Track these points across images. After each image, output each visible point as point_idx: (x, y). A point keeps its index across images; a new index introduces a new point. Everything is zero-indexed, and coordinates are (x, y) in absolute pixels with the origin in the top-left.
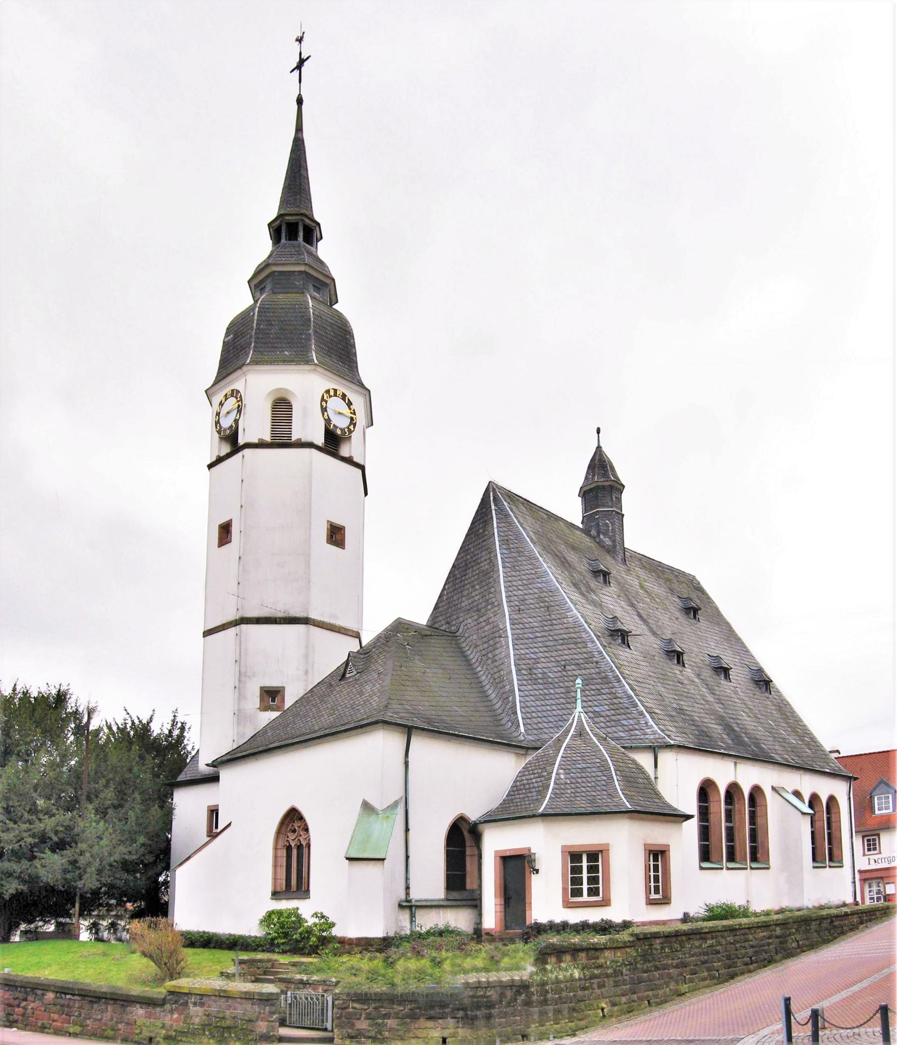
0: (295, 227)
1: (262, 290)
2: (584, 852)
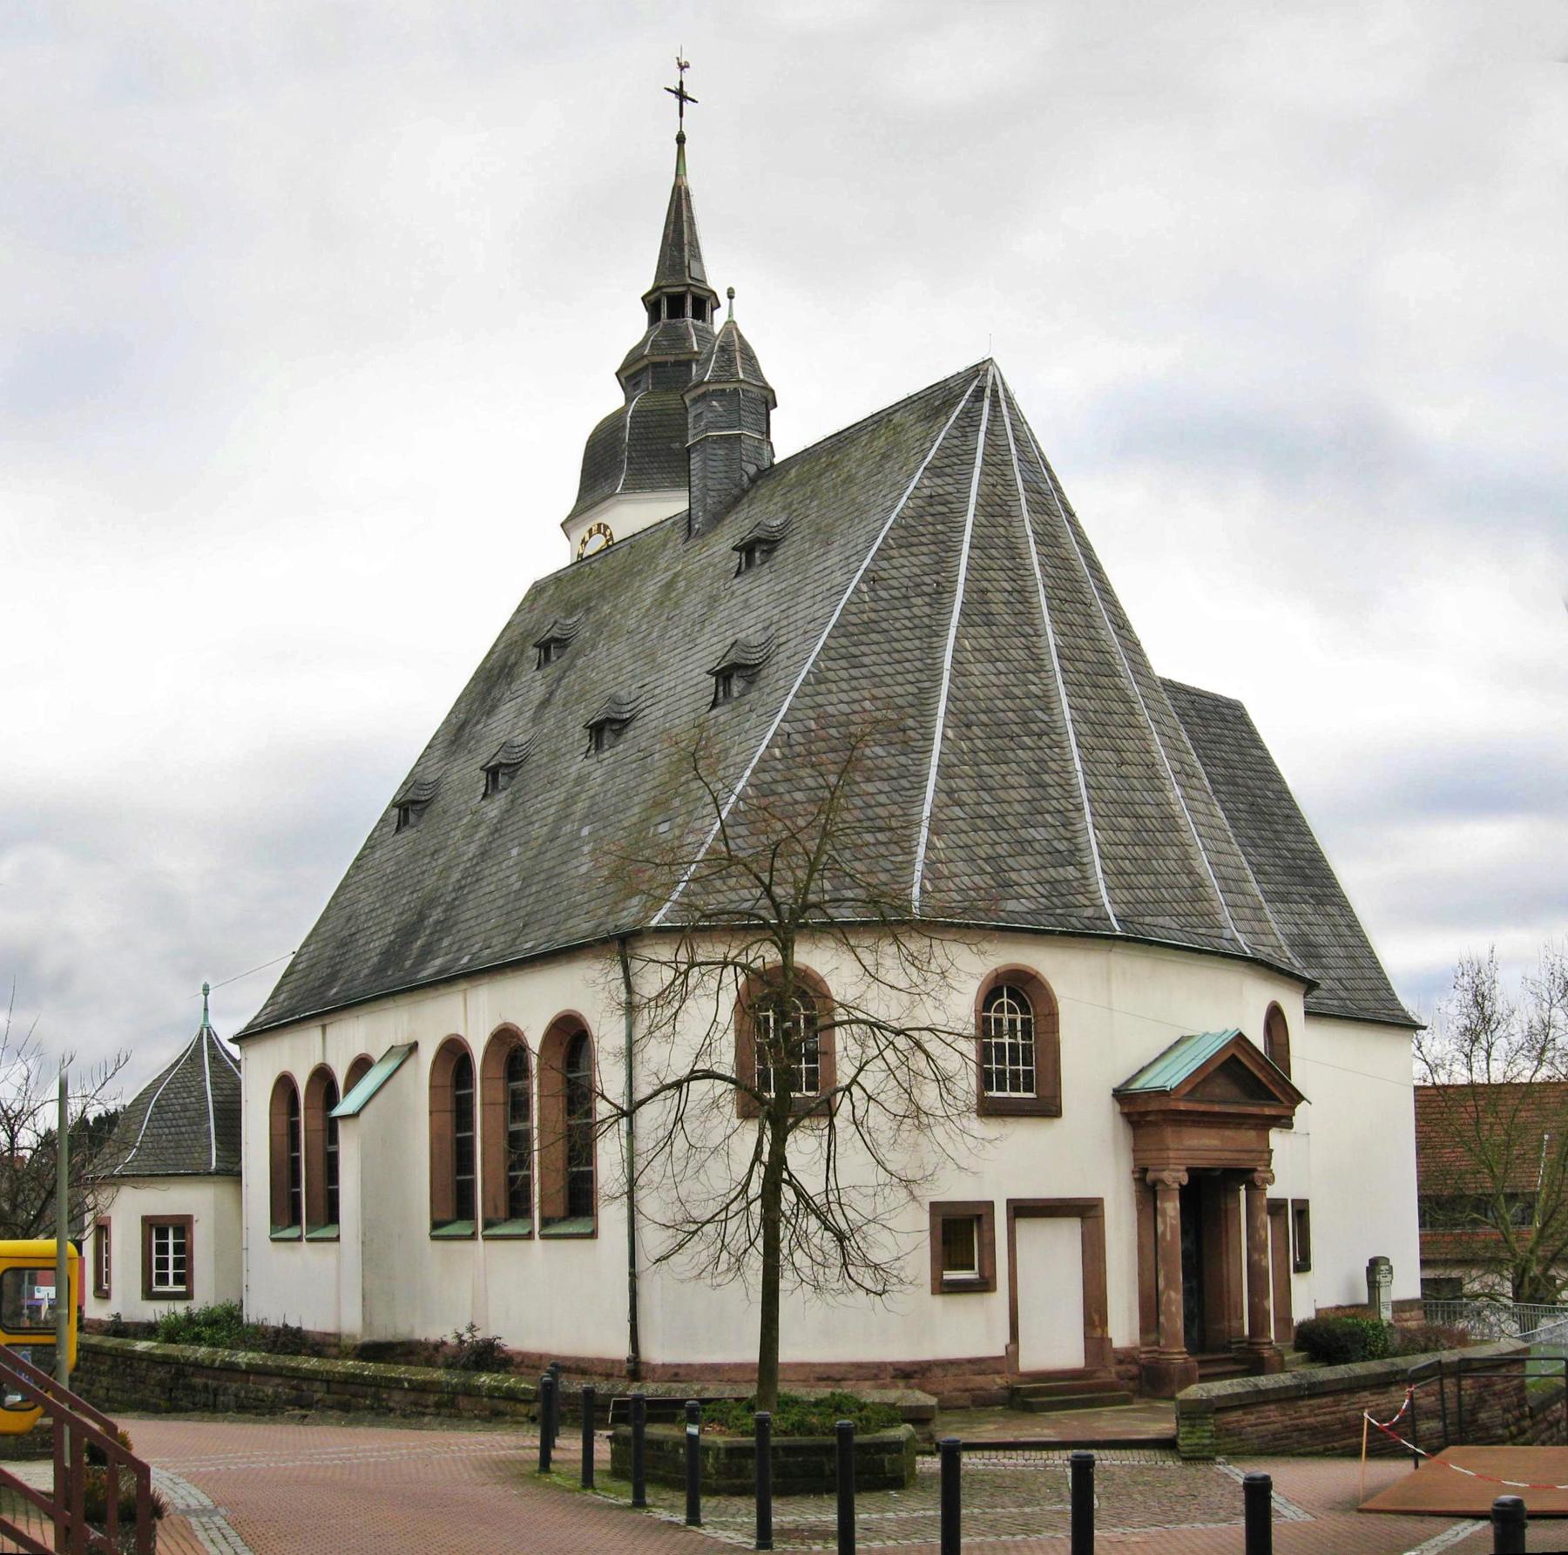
0: (678, 297)
1: (636, 385)
2: (506, 1127)
